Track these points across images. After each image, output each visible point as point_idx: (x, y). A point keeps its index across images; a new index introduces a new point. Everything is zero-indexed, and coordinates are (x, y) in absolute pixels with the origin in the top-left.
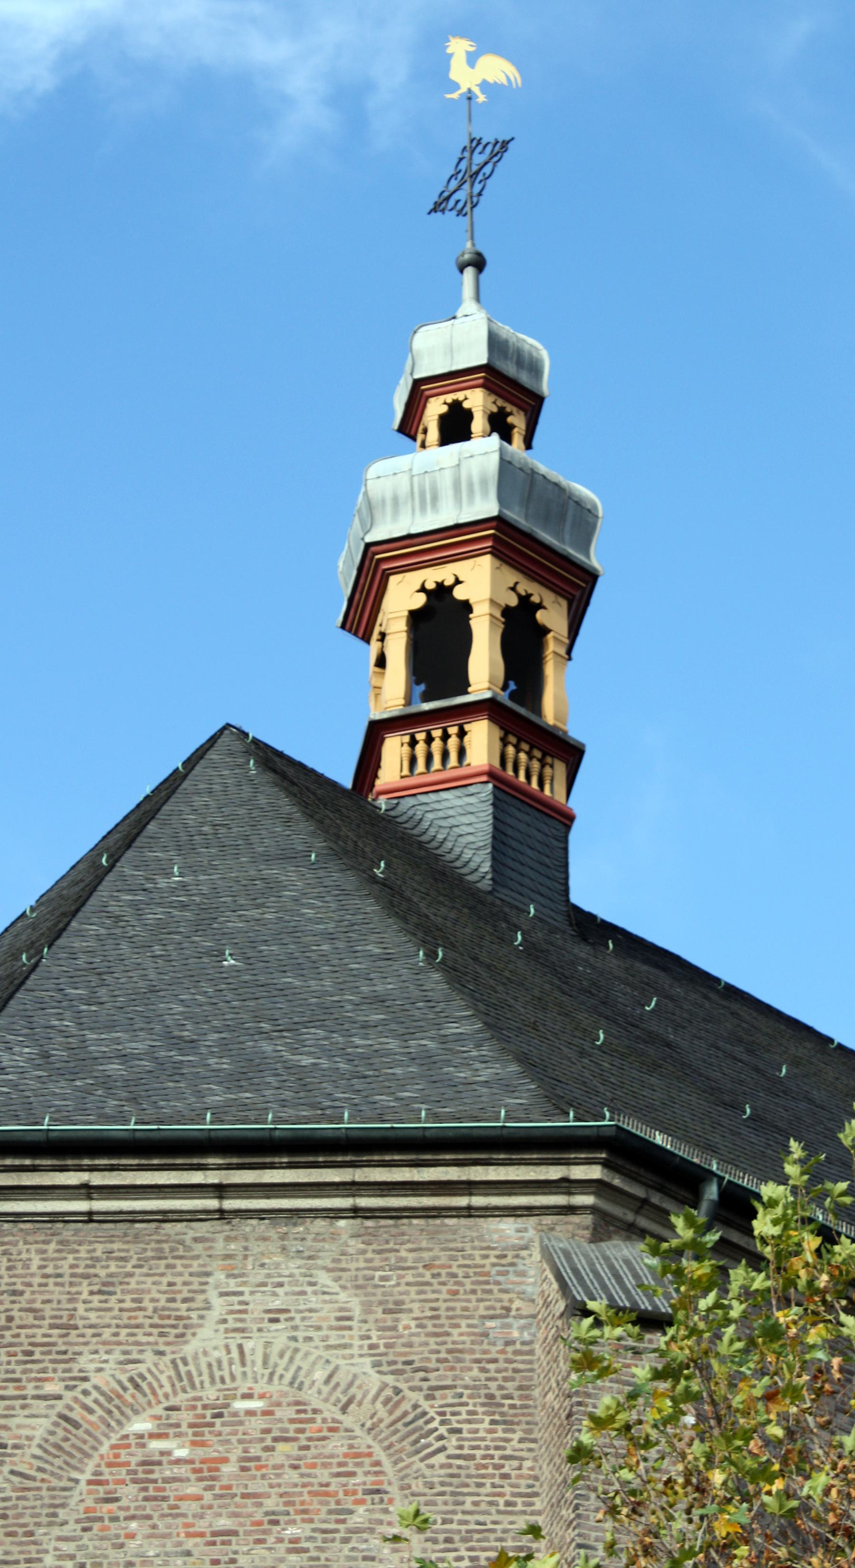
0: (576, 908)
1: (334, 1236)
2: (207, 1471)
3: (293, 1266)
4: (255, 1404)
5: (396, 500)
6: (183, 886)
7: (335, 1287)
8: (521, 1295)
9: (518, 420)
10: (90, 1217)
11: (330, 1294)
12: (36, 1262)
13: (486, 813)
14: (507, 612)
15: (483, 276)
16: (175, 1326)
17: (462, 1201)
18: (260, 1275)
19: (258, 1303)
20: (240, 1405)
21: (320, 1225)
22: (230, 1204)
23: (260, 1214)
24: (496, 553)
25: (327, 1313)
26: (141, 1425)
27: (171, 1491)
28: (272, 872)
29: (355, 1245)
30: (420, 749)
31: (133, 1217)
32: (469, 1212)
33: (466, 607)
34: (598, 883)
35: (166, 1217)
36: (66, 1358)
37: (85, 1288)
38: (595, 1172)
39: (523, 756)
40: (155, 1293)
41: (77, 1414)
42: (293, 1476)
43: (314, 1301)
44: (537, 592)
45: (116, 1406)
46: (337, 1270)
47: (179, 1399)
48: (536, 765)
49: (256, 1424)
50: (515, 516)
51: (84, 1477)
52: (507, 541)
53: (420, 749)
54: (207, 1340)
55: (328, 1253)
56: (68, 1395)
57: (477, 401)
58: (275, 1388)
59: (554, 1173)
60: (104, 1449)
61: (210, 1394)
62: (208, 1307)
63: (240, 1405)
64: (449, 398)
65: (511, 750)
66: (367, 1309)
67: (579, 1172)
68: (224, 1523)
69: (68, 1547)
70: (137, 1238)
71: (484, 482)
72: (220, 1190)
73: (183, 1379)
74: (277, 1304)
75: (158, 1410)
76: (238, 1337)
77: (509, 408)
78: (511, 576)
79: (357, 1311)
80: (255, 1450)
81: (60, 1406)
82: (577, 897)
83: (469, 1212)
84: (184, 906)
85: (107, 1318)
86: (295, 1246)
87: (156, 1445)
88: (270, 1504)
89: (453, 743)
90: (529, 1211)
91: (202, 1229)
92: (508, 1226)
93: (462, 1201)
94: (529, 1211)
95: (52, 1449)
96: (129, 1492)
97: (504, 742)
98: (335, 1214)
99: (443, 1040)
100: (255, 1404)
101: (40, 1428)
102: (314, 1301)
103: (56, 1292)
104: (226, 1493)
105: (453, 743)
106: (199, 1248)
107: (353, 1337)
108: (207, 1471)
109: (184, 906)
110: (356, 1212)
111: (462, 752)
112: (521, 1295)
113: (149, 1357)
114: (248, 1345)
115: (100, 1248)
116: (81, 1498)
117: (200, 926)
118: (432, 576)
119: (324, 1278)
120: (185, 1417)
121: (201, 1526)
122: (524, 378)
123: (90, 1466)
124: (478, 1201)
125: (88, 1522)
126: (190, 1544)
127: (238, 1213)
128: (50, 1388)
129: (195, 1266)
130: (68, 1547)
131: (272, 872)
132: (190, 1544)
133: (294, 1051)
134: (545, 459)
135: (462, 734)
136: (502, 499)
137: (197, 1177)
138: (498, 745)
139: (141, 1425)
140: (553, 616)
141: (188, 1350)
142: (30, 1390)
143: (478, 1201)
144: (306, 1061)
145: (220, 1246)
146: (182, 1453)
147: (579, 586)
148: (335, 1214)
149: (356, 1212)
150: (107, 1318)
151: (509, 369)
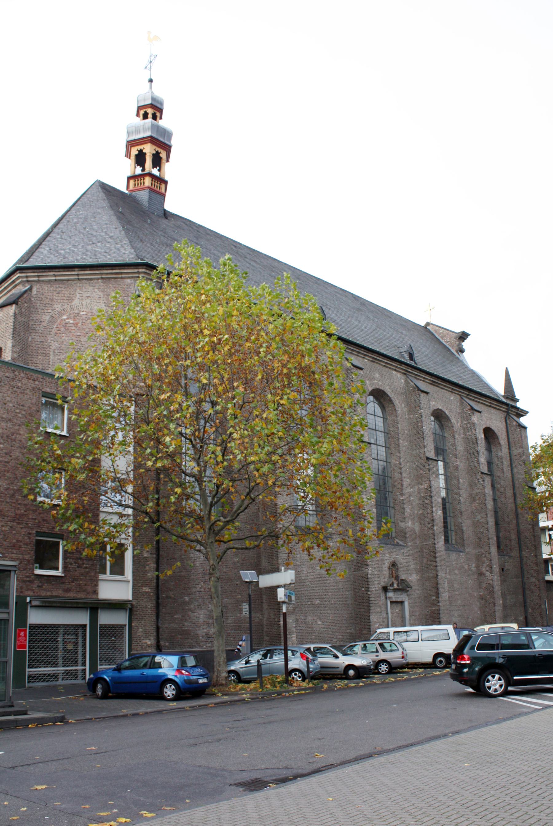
0: (165, 210)
1: (98, 283)
2: (76, 325)
3: (91, 288)
4: (84, 313)
5: (132, 132)
6: (82, 214)
7: (98, 292)
8: (131, 292)
9: (158, 114)
10: (56, 280)
11: (97, 293)
12: (46, 288)
13: (148, 194)
14: (153, 155)
15: (153, 84)
16: (70, 299)
17: (120, 276)
18: (85, 290)
19: (85, 295)
20: (82, 313)
21: (96, 281)
22: (80, 277)
23: (85, 279)
24: (151, 143)
25: (97, 297)
26: (65, 317)
27: (70, 328)
28: (99, 211)
29: (102, 284)
30: (136, 182)
31: (63, 280)
32: (122, 278)
33: (145, 154)
34: (170, 205)
35: (69, 280)
36: (52, 305)
37: (55, 293)
38: (144, 270)
39: (156, 184)
40: (67, 294)
41: (54, 315)
42: (90, 325)
43: (94, 294)
44: (160, 150)
45: (60, 314)
46: (99, 289)
47: (71, 312)
48: (159, 185)
49: (84, 317)
50: (155, 135)
51: (55, 326)
52: (152, 140)
53: (136, 182)
54: (76, 302)
55: (97, 285)
56: (52, 312)
57: (150, 111)
58: (88, 310)
59: (136, 271)
60: (59, 321)
61: (77, 311)
62: (76, 296)
63: (82, 313)
64: (144, 110)
65: (153, 182)
66: (104, 295)
67: (140, 270)
68: (79, 334)
69: (52, 339)
70: (64, 284)
71: (149, 129)
72: (78, 275)
73: (72, 309)
74: (88, 295)
75: (68, 314)
76: (81, 301)
77: (156, 112)
78: (154, 147)
79: (102, 296)
80: (84, 321)
81: (51, 314)
82: (165, 208)
83: (122, 278)
84: (81, 218)
85: (59, 298)
86: (92, 284)
87: (67, 321)
88: (87, 330)
89: (142, 181)
90: (132, 277)
91: (75, 282)
92: (129, 281)
93: (120, 276)
94: (132, 277)
95: (50, 322)
96: (63, 329)
97: (152, 181)
98: (98, 279)
99: (122, 245)
100: (84, 313)
101: (47, 318)
102: (94, 294)
103: (50, 294)
104: (79, 329)
105: (142, 181)
106: (75, 285)
107: (101, 301)
108: (76, 325)
109: (81, 218)
110: (102, 278)
111: (144, 183)
112: (131, 292)
113: (66, 305)
114: (83, 303)
115: (57, 286)
116: (54, 330)
117: (83, 223)
118: (139, 148)
119: (96, 290)
120: (72, 316)
121: (75, 334)
122: (159, 106)
123: (56, 324)
124: (123, 276)
125: (56, 334)
126: (73, 338)
127: (82, 279)
128: (49, 311)
129: (74, 288)
130: (52, 339)
131: (99, 211)
132: (73, 338)
133: (95, 248)
134: (161, 123)
135: (144, 179)
136: (152, 132)
137: (73, 273)
138: (151, 182)
139: (65, 317)
140: (163, 155)
141: (73, 304)
142: (46, 311)
143: (123, 276)
144: (97, 249)
145: (78, 285)
146: (71, 322)
147: (168, 148)
148: (98, 279)
149: (102, 278)
150: (59, 298)
151: (156, 104)
